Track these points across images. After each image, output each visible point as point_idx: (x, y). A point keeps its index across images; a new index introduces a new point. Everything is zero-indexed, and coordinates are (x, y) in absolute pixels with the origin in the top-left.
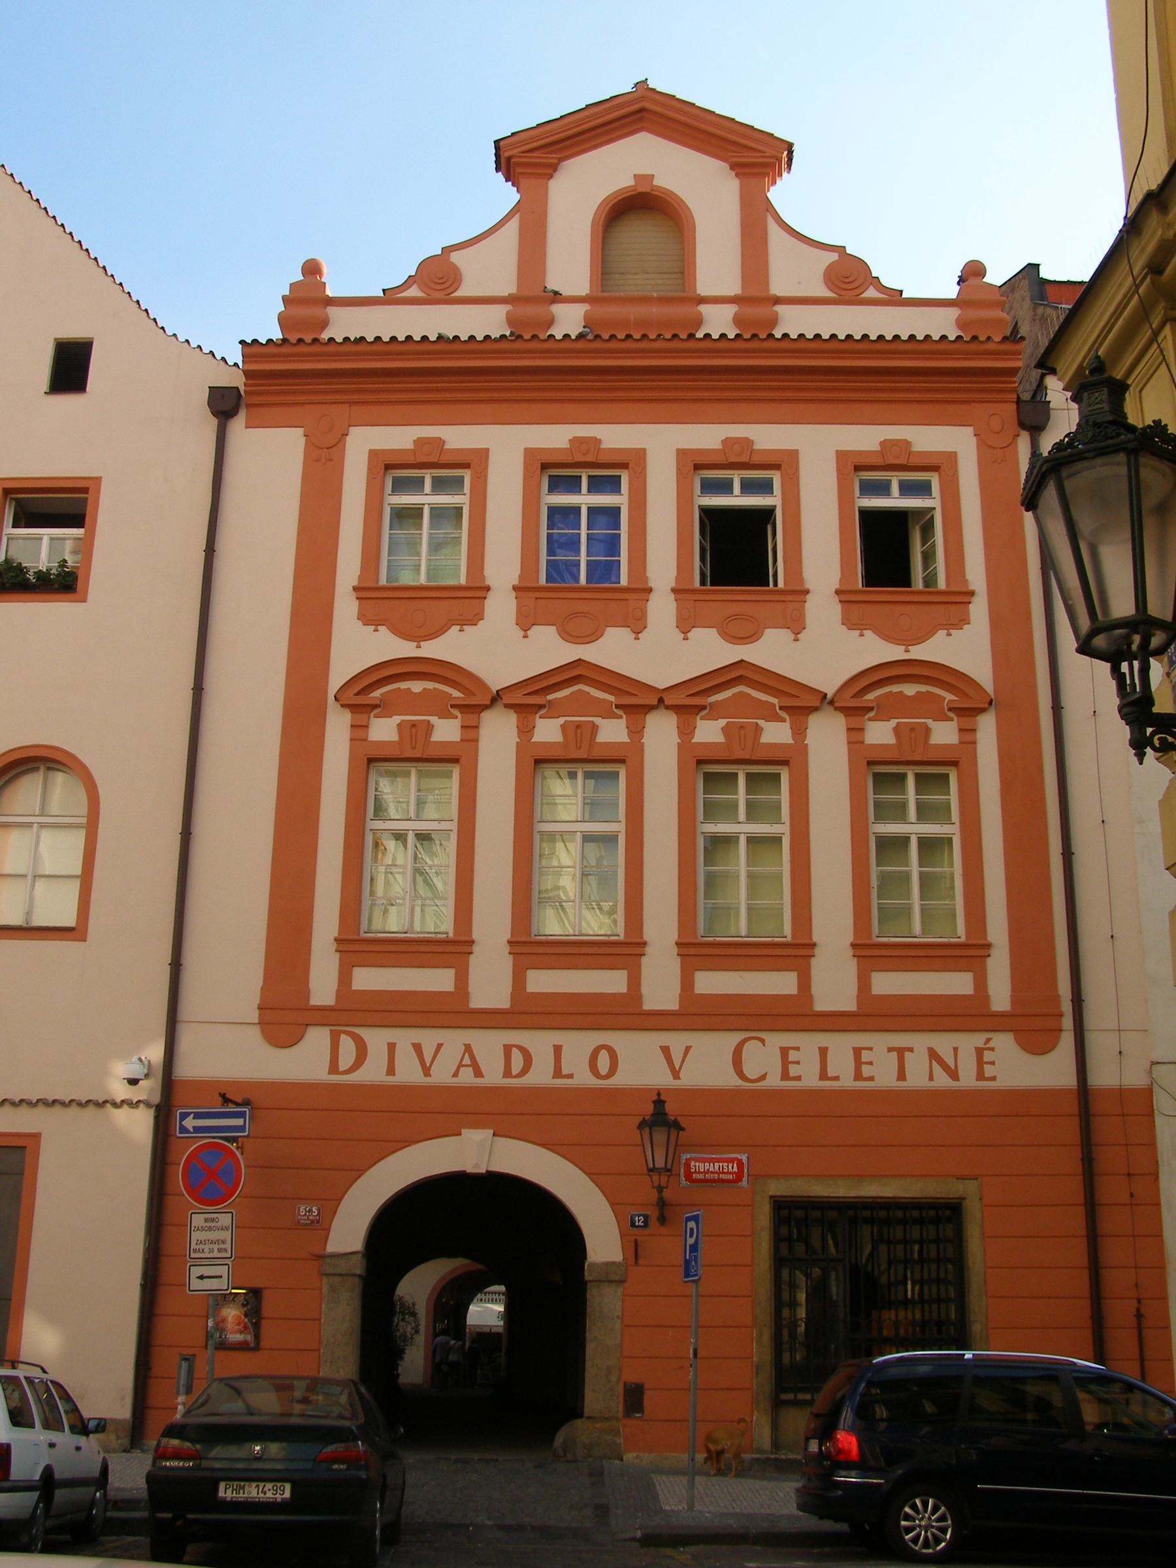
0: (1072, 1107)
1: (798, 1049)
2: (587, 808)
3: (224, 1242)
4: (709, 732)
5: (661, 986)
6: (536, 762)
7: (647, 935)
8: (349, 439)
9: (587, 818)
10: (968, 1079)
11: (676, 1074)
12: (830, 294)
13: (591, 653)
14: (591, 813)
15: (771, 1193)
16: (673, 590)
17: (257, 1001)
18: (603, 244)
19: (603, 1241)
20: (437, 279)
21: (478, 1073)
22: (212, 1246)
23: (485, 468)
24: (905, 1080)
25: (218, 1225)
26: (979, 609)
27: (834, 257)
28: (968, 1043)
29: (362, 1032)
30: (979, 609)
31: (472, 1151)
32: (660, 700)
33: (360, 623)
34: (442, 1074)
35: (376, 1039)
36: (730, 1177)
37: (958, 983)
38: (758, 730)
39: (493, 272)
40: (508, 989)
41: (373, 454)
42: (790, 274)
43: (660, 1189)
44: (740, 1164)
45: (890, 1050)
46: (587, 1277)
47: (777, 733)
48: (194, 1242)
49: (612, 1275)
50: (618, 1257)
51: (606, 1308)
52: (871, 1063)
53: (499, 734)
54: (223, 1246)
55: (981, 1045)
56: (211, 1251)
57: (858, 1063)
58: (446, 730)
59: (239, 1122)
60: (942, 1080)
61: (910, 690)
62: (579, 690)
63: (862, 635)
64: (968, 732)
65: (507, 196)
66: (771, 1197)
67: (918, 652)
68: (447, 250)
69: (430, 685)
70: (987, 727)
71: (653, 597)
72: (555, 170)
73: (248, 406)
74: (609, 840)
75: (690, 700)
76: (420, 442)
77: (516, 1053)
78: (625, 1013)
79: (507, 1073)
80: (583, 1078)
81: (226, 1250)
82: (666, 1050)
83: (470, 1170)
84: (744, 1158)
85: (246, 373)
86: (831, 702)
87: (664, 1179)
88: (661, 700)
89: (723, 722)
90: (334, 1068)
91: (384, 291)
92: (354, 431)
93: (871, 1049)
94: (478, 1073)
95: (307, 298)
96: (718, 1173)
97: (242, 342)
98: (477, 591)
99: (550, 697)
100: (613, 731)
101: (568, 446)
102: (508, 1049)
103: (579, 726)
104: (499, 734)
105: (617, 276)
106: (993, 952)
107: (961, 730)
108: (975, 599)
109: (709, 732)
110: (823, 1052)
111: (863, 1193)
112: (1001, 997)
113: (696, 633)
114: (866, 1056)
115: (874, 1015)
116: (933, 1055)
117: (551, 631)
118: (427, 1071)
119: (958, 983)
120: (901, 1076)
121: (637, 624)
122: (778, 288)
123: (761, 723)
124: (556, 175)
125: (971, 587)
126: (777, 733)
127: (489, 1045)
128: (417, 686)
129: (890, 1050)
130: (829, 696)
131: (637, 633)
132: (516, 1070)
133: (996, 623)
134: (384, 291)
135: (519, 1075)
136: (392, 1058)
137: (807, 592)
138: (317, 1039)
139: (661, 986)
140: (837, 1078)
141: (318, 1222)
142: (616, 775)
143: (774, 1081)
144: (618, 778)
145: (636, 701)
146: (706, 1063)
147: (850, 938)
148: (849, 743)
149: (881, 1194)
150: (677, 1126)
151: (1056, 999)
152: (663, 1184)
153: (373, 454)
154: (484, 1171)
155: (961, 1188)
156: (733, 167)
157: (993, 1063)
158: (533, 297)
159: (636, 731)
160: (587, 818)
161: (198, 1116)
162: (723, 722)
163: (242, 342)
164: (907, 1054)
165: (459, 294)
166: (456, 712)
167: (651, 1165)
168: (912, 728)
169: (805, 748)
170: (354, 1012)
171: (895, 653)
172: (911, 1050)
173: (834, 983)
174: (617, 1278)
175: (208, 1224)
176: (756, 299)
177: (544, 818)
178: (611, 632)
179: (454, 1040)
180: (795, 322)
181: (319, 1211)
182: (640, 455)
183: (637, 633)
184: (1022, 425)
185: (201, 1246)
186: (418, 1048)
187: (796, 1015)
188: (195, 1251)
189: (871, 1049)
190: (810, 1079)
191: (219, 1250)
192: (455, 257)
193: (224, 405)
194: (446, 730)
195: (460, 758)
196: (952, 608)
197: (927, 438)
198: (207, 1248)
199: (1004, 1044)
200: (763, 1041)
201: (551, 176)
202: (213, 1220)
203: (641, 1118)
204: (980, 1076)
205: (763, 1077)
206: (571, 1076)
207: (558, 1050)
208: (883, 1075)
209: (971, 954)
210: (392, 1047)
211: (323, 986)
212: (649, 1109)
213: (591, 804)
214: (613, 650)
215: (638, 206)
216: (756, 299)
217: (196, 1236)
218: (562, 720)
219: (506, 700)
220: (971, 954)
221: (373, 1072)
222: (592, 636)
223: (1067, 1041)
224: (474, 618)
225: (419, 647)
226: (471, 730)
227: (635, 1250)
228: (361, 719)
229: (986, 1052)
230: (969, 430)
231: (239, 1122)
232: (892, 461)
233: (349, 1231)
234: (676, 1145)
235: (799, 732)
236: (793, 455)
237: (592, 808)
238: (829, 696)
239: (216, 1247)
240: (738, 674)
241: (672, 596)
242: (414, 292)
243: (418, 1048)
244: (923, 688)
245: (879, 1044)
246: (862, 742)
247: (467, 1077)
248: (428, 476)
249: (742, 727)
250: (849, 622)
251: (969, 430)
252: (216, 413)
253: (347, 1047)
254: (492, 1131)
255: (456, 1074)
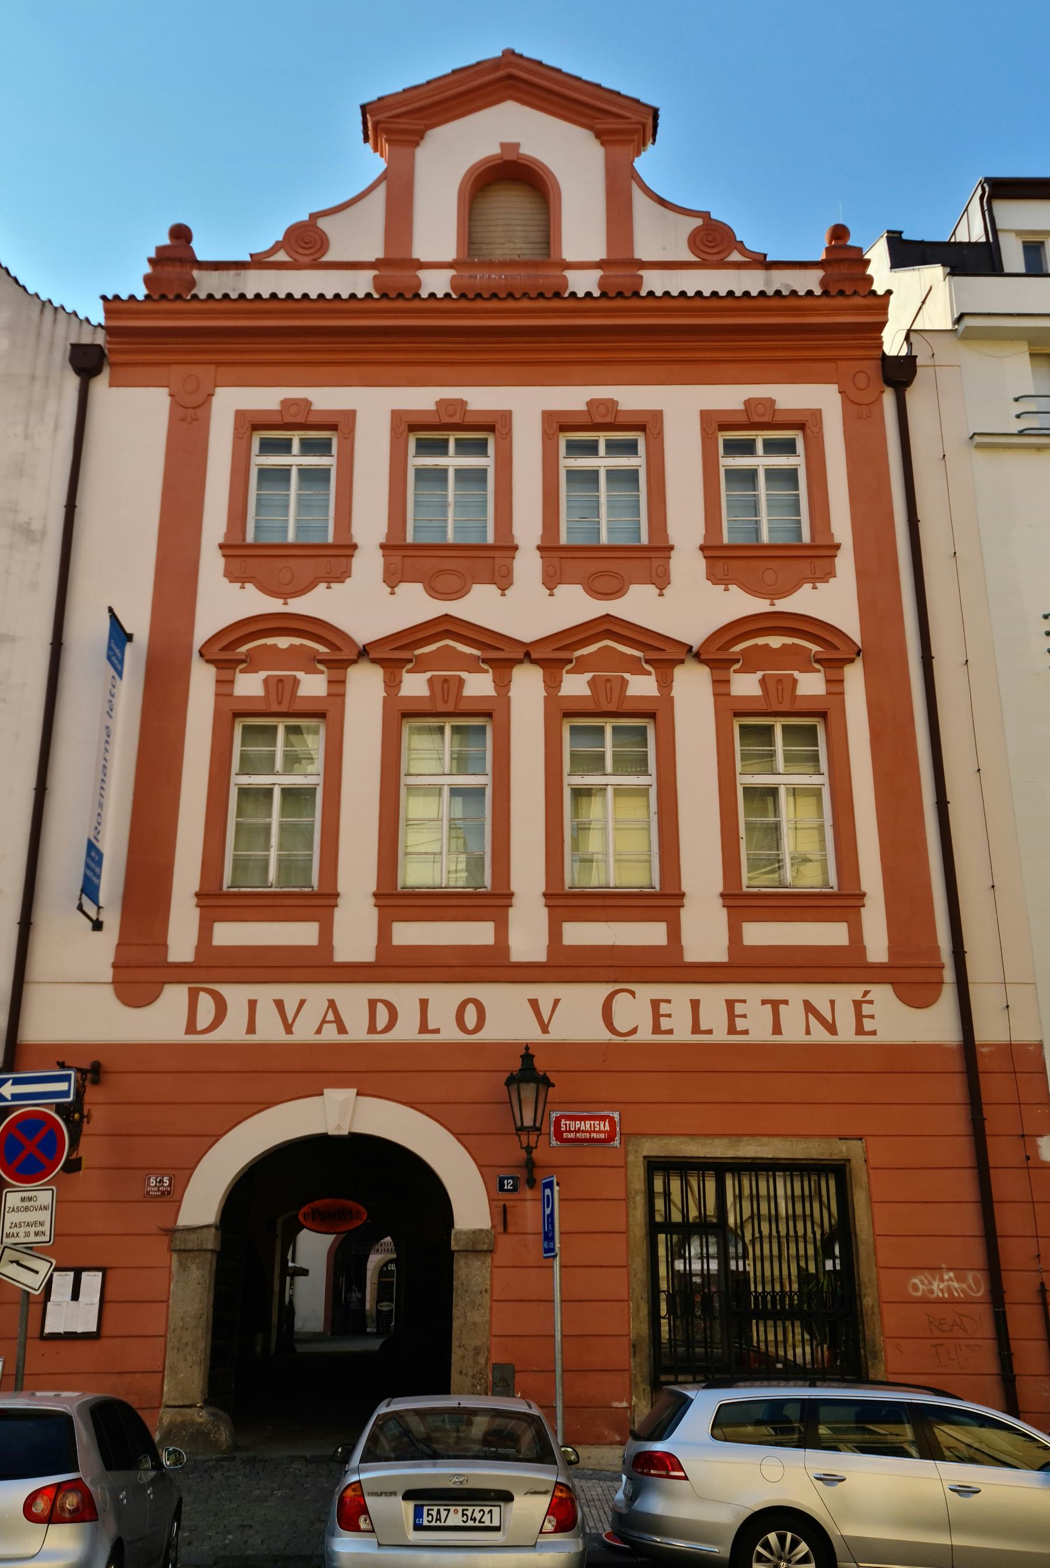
0: (957, 1064)
1: (669, 1001)
2: (455, 762)
3: (42, 1224)
4: (575, 685)
5: (528, 937)
6: (400, 715)
7: (515, 886)
8: (215, 400)
9: (454, 772)
10: (846, 1034)
11: (545, 1029)
12: (693, 258)
13: (459, 609)
14: (459, 766)
15: (645, 1153)
16: (539, 548)
17: (111, 959)
18: (470, 220)
19: (471, 1207)
20: (306, 243)
21: (342, 1029)
22: (28, 1229)
23: (352, 430)
24: (780, 1033)
25: (37, 1204)
26: (845, 563)
27: (698, 222)
28: (846, 995)
29: (223, 989)
30: (845, 563)
31: (334, 1112)
32: (527, 653)
33: (226, 580)
34: (304, 1032)
35: (236, 995)
36: (602, 1136)
37: (831, 934)
38: (624, 683)
39: (361, 238)
40: (373, 942)
41: (240, 415)
42: (657, 238)
43: (529, 1149)
44: (612, 1121)
45: (764, 1002)
46: (454, 1247)
47: (642, 686)
48: (7, 1225)
49: (480, 1246)
50: (485, 1223)
51: (471, 1276)
52: (744, 1016)
53: (365, 685)
54: (40, 1229)
55: (859, 998)
56: (27, 1234)
57: (732, 1016)
58: (313, 685)
59: (63, 1086)
60: (820, 1035)
61: (776, 642)
62: (447, 646)
63: (726, 590)
64: (835, 684)
65: (373, 164)
66: (645, 1157)
67: (784, 605)
68: (314, 217)
69: (297, 641)
70: (854, 676)
71: (518, 554)
72: (422, 138)
73: (111, 365)
74: (475, 794)
75: (553, 654)
76: (286, 403)
77: (381, 1009)
78: (492, 965)
79: (372, 1029)
80: (451, 1033)
81: (43, 1233)
82: (534, 1004)
83: (332, 1132)
84: (616, 1116)
85: (109, 330)
86: (697, 656)
87: (533, 1138)
88: (527, 655)
89: (588, 676)
90: (191, 1027)
91: (251, 255)
92: (220, 392)
93: (744, 1001)
94: (342, 1029)
95: (176, 256)
96: (590, 1132)
97: (104, 298)
98: (346, 549)
99: (578, 653)
100: (479, 685)
101: (434, 408)
102: (372, 1004)
103: (446, 680)
104: (365, 685)
105: (484, 246)
106: (867, 901)
107: (828, 681)
108: (840, 553)
109: (575, 685)
110: (695, 1004)
111: (741, 1154)
112: (877, 947)
113: (562, 590)
114: (739, 1009)
115: (745, 966)
116: (809, 1007)
117: (419, 587)
118: (288, 1028)
119: (831, 934)
120: (777, 1029)
121: (503, 581)
122: (643, 252)
123: (627, 676)
124: (422, 143)
125: (837, 541)
126: (642, 686)
127: (352, 1000)
128: (283, 642)
129: (764, 1002)
130: (695, 649)
131: (503, 590)
132: (380, 1026)
133: (862, 575)
134: (251, 255)
135: (382, 1032)
136: (255, 1015)
137: (672, 548)
138: (174, 997)
139: (528, 937)
140: (710, 1032)
141: (169, 1193)
142: (483, 729)
143: (645, 1035)
144: (485, 733)
145: (501, 654)
146: (577, 1015)
147: (719, 887)
148: (715, 695)
149: (760, 1155)
150: (545, 1082)
151: (937, 949)
152: (532, 1144)
153: (240, 415)
154: (346, 1133)
155: (844, 1148)
156: (599, 135)
157: (872, 1017)
158: (397, 263)
159: (503, 684)
160: (454, 772)
161: (17, 1082)
162: (588, 676)
163: (104, 298)
164: (782, 1007)
165: (326, 258)
166: (321, 667)
167: (519, 1124)
168: (780, 680)
169: (671, 700)
170: (214, 967)
171: (761, 606)
172: (786, 1002)
173: (705, 934)
174: (485, 1247)
175: (25, 1204)
176: (621, 263)
177: (412, 771)
178: (477, 589)
179: (317, 995)
180: (654, 282)
181: (170, 1180)
182: (506, 416)
183: (503, 590)
184: (888, 381)
185: (15, 1230)
186: (280, 1004)
187: (667, 966)
188: (8, 1236)
189: (744, 1001)
190: (682, 1033)
191: (36, 1234)
192: (322, 224)
193: (87, 362)
194: (313, 685)
195: (327, 713)
196: (817, 562)
197: (790, 396)
198: (22, 1231)
199: (882, 995)
200: (633, 993)
201: (416, 144)
202: (30, 1199)
203: (507, 1075)
204: (860, 1030)
205: (634, 1031)
206: (437, 1031)
207: (424, 1004)
208: (757, 1028)
209: (842, 902)
210: (252, 1004)
211: (181, 943)
212: (517, 1065)
213: (457, 759)
214: (480, 606)
215: (511, 176)
216: (621, 263)
217: (10, 1218)
218: (429, 674)
219: (372, 655)
220: (842, 902)
221: (232, 1031)
222: (458, 593)
223: (948, 995)
224: (342, 575)
225: (286, 604)
226: (337, 685)
227: (503, 1216)
228: (226, 675)
229: (864, 1006)
230: (834, 388)
231: (63, 1086)
232: (756, 419)
233: (202, 1202)
234: (545, 1103)
235: (665, 684)
236: (657, 416)
237: (462, 763)
238: (695, 649)
239: (32, 1230)
240: (607, 627)
241: (380, 552)
242: (282, 256)
243: (280, 1004)
244: (789, 640)
245: (752, 996)
246: (729, 694)
247: (330, 1034)
248: (296, 437)
249: (608, 680)
250: (713, 577)
251: (834, 388)
252: (78, 370)
253: (206, 1006)
254: (355, 1091)
255: (319, 1031)
